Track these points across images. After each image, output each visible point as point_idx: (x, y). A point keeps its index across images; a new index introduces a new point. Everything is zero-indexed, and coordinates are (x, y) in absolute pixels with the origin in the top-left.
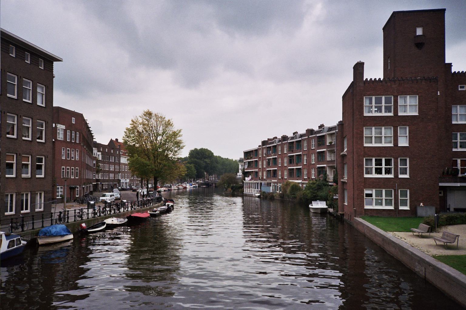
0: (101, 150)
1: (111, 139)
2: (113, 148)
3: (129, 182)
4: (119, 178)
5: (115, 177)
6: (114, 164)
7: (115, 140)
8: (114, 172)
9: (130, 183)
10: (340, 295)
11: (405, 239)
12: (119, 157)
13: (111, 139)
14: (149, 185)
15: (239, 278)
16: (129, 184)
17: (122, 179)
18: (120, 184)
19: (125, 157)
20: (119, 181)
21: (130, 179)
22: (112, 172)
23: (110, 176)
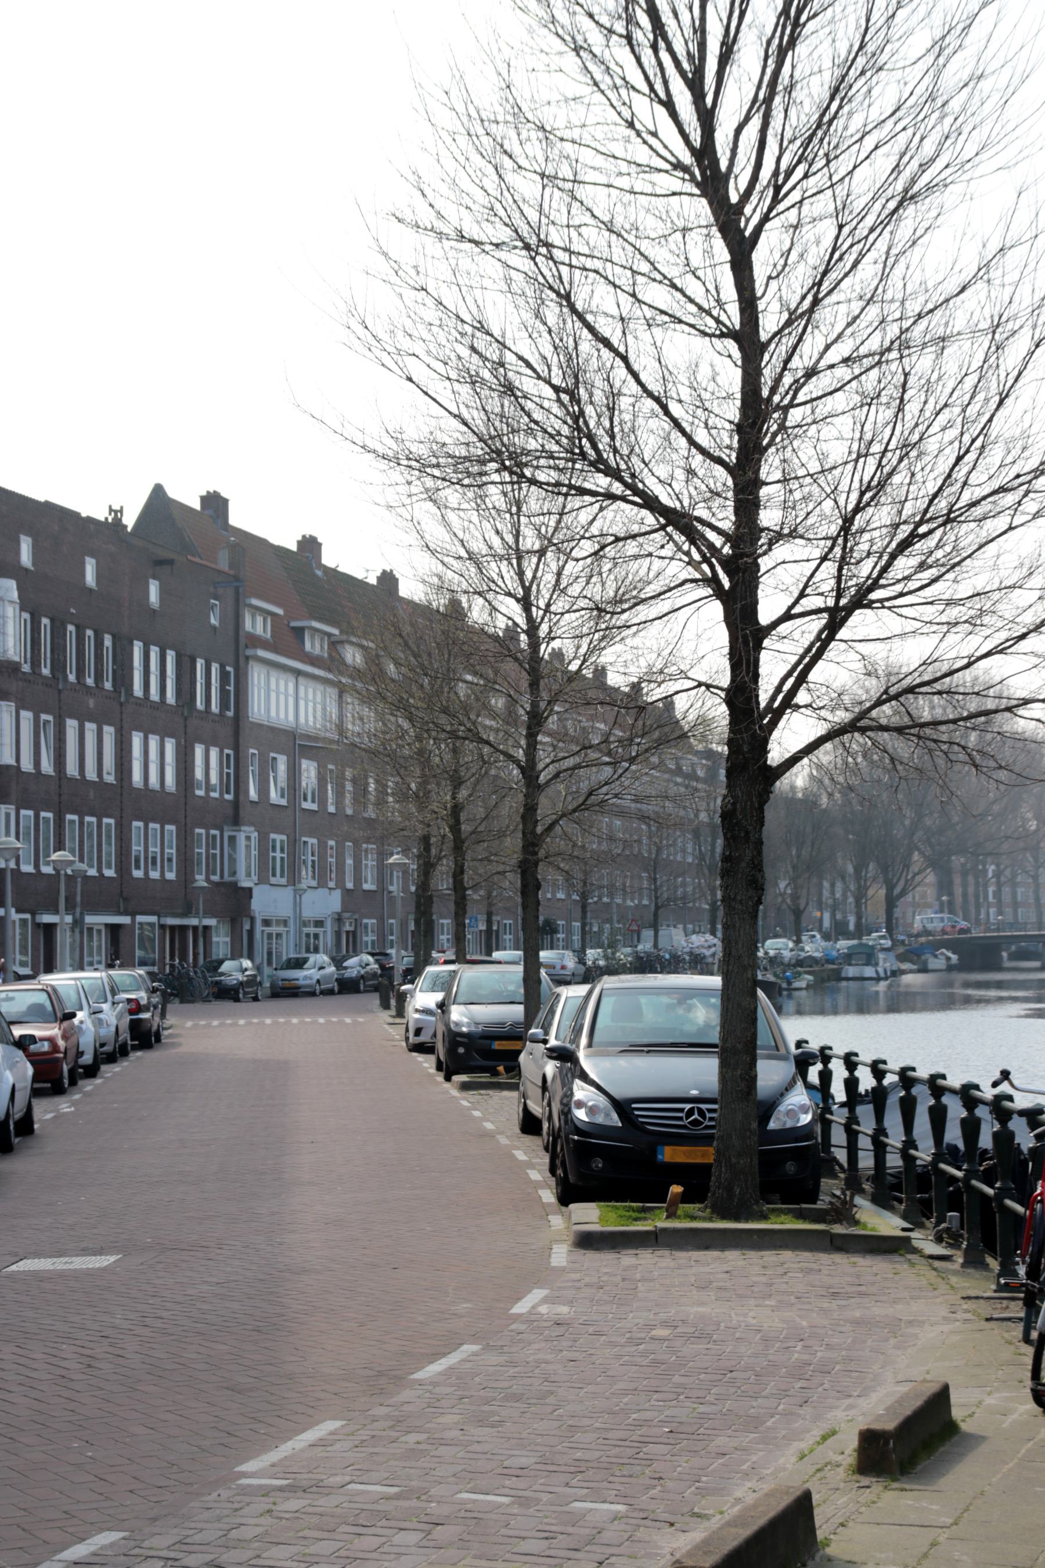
0: (26, 557)
1: (158, 491)
2: (160, 563)
3: (339, 919)
4: (234, 873)
5: (186, 862)
6: (182, 723)
7: (196, 505)
8: (180, 807)
9: (348, 927)
10: (141, 734)
11: (802, 1457)
12: (236, 655)
13: (158, 491)
14: (900, 1163)
15: (779, 29)
16: (338, 934)
17: (263, 880)
18: (251, 933)
19: (298, 673)
20: (234, 902)
21: (347, 893)
22: (152, 806)
23: (137, 848)
